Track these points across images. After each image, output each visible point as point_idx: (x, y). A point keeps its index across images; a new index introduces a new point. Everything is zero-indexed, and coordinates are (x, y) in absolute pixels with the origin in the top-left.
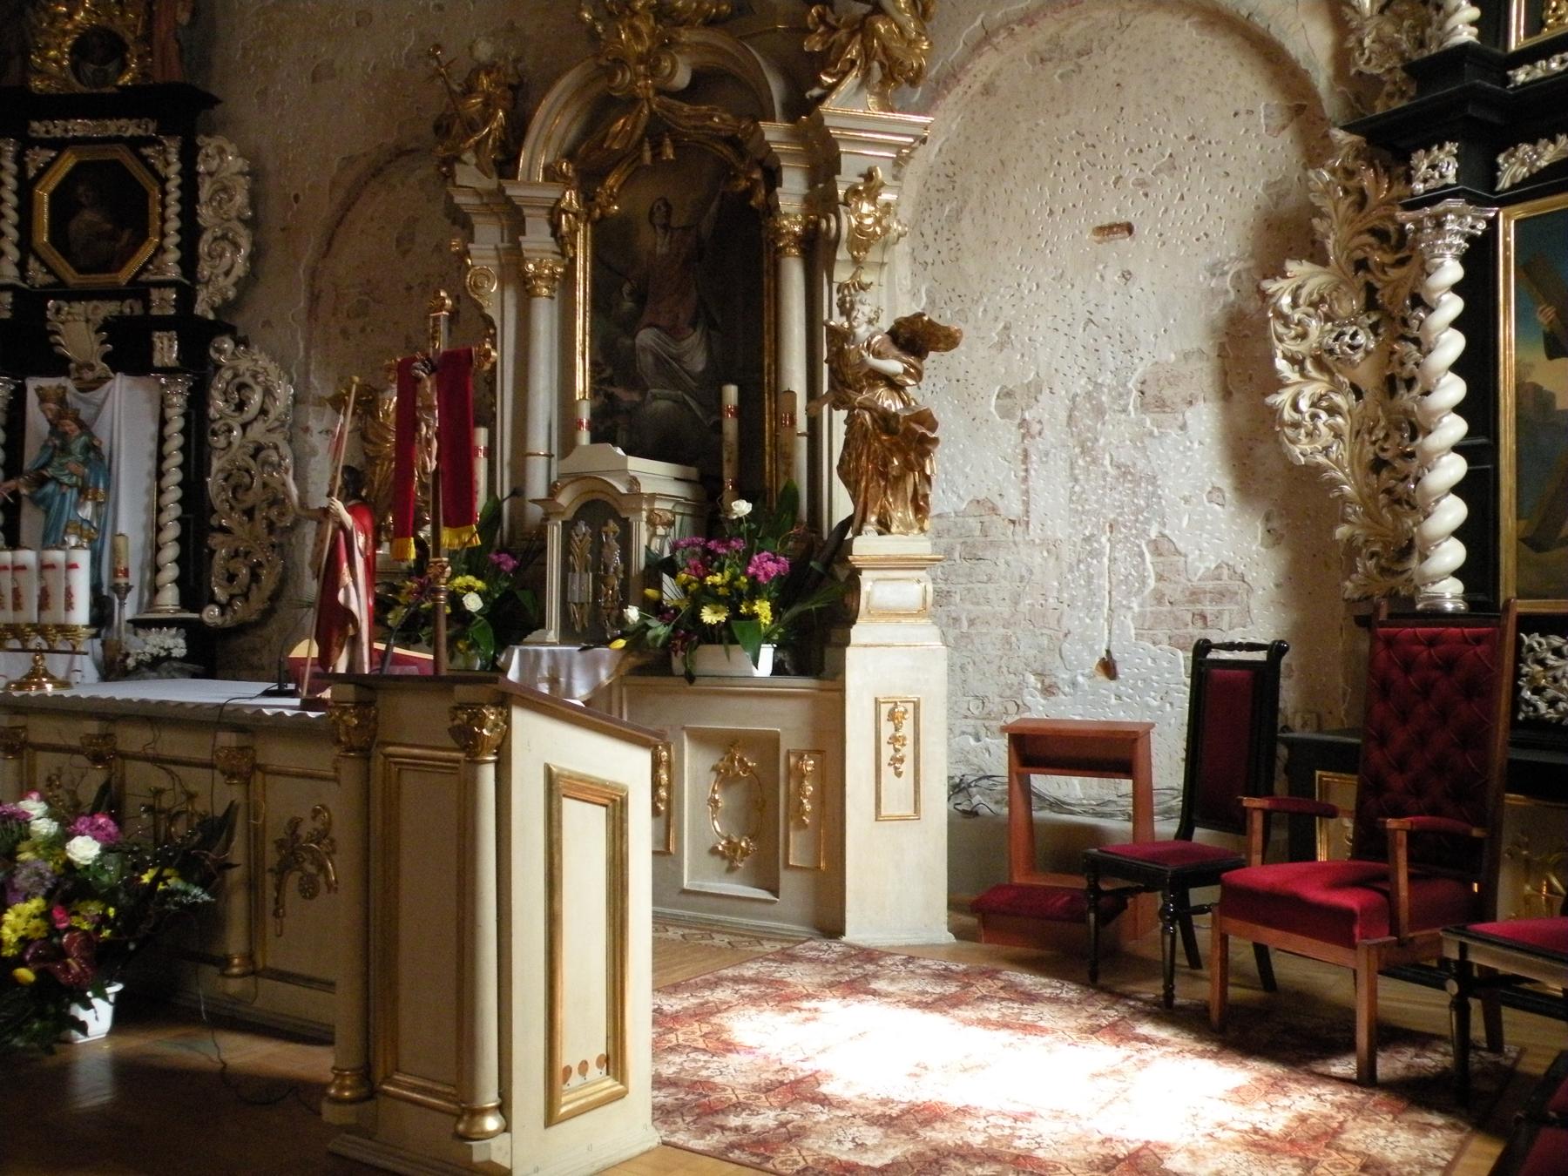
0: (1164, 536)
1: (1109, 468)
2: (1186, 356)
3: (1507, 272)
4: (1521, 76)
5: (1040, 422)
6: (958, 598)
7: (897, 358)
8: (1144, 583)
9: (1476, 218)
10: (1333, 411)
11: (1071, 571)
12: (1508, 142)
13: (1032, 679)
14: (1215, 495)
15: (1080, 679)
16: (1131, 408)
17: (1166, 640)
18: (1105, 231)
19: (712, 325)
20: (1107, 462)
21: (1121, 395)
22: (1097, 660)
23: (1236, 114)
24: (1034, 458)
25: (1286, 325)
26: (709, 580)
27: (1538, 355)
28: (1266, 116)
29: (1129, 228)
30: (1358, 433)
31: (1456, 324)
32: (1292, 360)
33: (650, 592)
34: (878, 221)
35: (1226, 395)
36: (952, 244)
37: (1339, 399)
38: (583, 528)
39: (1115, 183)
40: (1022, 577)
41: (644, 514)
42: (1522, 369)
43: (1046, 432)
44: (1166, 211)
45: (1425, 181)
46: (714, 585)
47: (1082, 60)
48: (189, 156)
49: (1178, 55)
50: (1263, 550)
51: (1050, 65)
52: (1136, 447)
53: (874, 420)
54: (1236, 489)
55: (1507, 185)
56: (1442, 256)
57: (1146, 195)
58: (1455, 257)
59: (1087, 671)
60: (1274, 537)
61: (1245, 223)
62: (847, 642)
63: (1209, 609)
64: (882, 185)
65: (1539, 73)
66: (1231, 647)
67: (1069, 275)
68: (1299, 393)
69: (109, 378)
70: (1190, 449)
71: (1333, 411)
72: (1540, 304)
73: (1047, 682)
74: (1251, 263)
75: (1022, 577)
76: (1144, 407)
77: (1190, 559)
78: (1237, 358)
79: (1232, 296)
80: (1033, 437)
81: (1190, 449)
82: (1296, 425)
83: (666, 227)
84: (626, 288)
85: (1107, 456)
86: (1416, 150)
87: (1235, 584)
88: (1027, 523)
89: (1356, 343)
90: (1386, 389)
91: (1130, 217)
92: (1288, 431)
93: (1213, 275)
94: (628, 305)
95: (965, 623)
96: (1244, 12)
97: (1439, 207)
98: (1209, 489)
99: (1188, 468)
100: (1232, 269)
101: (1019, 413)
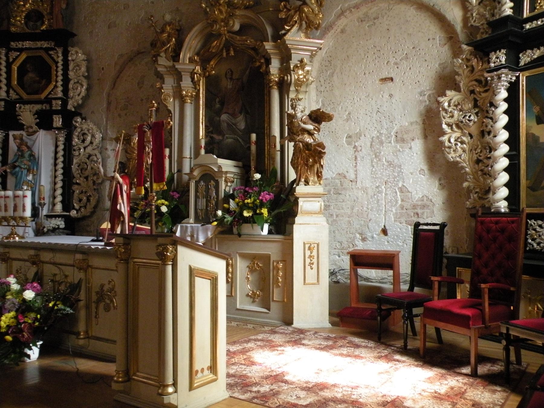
0: (404, 186)
1: (385, 163)
2: (412, 124)
3: (523, 94)
4: (528, 26)
5: (361, 146)
6: (332, 207)
7: (311, 124)
8: (397, 202)
9: (512, 76)
10: (462, 142)
11: (372, 198)
12: (523, 49)
13: (358, 236)
14: (421, 172)
15: (375, 236)
16: (392, 141)
17: (405, 222)
18: (384, 80)
19: (247, 113)
20: (384, 160)
21: (389, 137)
22: (381, 229)
23: (429, 40)
24: (359, 159)
25: (446, 113)
26: (246, 201)
27: (534, 123)
28: (439, 40)
29: (392, 79)
30: (471, 150)
31: (505, 112)
32: (448, 125)
33: (225, 205)
34: (305, 77)
35: (425, 137)
36: (330, 85)
37: (464, 139)
38: (202, 183)
39: (387, 64)
40: (355, 200)
41: (224, 178)
42: (528, 128)
43: (363, 150)
44: (405, 73)
45: (494, 63)
46: (248, 203)
47: (375, 21)
48: (66, 54)
49: (409, 19)
50: (438, 191)
51: (364, 23)
52: (394, 155)
53: (303, 146)
54: (429, 170)
55: (523, 64)
56: (500, 89)
57: (398, 68)
58: (505, 89)
59: (377, 233)
60: (442, 186)
61: (432, 78)
62: (294, 223)
63: (419, 211)
64: (306, 64)
65: (534, 25)
66: (427, 224)
67: (371, 95)
68: (451, 136)
69: (38, 131)
70: (413, 156)
71: (462, 142)
72: (534, 105)
73: (363, 236)
74: (434, 91)
75: (355, 200)
76: (397, 141)
77: (413, 194)
78: (429, 124)
79: (427, 103)
80: (358, 152)
81: (413, 156)
82: (450, 148)
83: (231, 79)
84: (217, 100)
85: (384, 158)
86: (491, 52)
87: (429, 203)
88: (356, 181)
89: (470, 119)
90: (481, 135)
91: (392, 75)
92: (447, 150)
93: (421, 95)
94: (218, 106)
95: (335, 216)
96: (432, 4)
97: (499, 72)
98: (419, 169)
99: (412, 163)
100: (427, 93)
101: (353, 143)
